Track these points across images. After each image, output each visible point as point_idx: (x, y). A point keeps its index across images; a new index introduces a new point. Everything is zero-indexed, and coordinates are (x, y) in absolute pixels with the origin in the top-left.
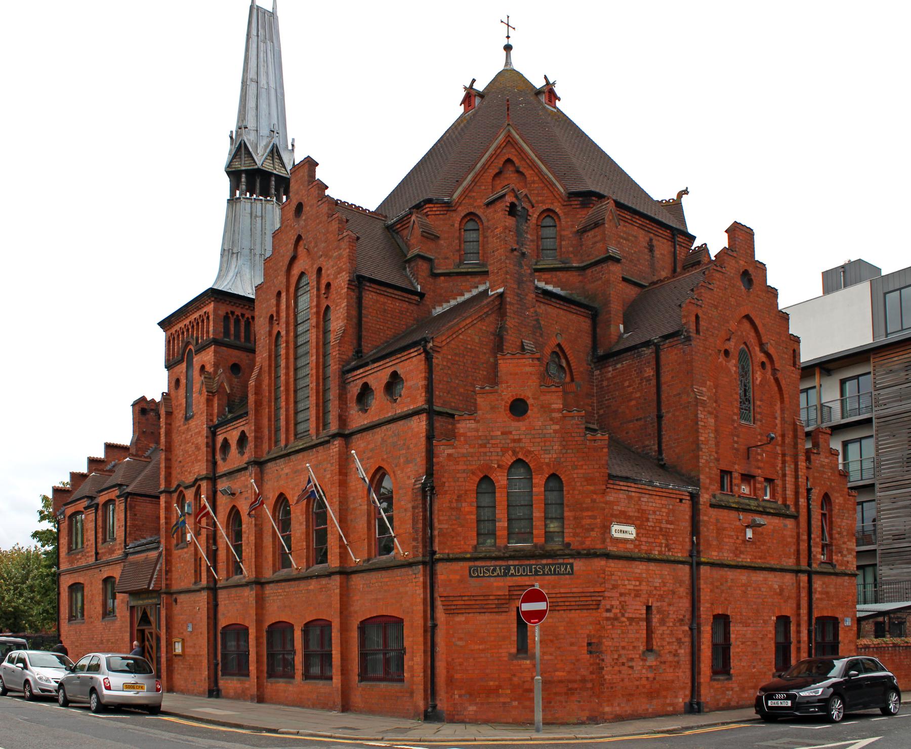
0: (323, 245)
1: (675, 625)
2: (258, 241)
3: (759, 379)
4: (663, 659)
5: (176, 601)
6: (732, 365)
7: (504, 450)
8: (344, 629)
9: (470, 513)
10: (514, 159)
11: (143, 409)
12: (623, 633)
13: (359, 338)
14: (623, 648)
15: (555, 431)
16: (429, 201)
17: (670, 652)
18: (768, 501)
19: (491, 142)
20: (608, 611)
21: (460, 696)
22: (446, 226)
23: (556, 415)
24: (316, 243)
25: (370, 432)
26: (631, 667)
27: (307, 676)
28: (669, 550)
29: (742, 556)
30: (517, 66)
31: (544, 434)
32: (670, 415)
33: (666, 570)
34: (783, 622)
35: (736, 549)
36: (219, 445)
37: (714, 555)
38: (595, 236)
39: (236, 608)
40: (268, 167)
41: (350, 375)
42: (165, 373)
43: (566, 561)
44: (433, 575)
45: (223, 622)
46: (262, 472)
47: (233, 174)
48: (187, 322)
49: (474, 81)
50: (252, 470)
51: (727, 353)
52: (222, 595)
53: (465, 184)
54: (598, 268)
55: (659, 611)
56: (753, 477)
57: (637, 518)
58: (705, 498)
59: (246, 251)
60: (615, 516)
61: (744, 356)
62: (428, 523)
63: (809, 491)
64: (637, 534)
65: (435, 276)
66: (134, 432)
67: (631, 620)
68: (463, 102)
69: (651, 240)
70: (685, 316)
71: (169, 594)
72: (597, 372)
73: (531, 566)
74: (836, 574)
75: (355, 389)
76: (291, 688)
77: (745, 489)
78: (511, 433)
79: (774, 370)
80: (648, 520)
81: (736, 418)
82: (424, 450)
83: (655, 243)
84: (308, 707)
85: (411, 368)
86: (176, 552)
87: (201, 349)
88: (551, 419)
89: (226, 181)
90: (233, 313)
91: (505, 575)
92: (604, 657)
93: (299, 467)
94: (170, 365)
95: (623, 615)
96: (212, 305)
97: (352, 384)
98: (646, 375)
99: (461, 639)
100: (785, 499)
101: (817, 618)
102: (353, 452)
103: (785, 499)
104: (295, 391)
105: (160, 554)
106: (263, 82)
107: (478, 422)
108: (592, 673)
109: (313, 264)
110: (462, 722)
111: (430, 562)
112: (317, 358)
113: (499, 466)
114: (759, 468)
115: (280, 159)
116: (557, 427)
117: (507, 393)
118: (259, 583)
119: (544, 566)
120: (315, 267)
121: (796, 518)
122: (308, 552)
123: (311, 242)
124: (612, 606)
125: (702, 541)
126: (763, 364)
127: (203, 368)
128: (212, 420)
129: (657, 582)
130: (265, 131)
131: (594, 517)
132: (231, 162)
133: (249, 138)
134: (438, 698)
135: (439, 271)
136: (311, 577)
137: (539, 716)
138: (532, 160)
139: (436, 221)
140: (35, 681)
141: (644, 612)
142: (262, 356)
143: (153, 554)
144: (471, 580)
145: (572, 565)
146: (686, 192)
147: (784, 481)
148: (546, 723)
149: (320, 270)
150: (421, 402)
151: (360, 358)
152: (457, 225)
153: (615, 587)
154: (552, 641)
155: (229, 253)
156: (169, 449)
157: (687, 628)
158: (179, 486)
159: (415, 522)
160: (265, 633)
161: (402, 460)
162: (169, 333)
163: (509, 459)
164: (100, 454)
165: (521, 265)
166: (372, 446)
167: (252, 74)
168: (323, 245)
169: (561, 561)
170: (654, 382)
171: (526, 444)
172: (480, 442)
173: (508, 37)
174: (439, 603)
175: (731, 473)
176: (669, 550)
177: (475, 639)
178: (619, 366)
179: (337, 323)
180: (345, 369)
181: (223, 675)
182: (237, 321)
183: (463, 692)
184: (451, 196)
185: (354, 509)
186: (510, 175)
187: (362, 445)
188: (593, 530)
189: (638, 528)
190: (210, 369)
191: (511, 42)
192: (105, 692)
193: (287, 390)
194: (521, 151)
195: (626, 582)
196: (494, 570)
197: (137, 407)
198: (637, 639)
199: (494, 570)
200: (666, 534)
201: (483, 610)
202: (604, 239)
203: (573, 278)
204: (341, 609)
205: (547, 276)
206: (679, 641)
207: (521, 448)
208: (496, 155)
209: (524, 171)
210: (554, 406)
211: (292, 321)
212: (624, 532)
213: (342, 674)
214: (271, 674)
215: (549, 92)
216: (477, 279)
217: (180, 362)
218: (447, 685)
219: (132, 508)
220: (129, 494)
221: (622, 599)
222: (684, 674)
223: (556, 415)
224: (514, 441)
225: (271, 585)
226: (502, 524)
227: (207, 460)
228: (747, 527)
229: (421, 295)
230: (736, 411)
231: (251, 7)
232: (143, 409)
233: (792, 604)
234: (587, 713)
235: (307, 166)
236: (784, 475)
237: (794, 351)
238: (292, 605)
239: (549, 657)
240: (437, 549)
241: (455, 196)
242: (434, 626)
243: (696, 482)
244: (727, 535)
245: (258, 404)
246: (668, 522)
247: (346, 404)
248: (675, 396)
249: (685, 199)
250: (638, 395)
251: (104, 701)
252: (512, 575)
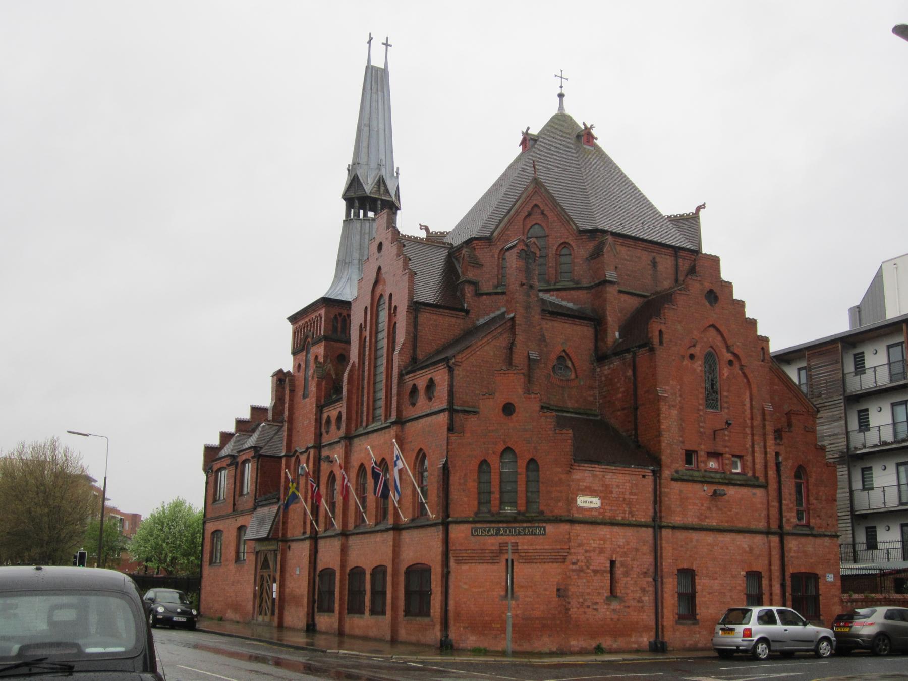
1: (638, 577)
3: (726, 375)
4: (627, 604)
5: (289, 548)
6: (698, 366)
8: (395, 574)
11: (281, 378)
12: (588, 582)
13: (415, 347)
14: (589, 594)
17: (634, 599)
18: (737, 474)
20: (574, 564)
26: (596, 610)
28: (632, 516)
29: (707, 520)
30: (568, 111)
33: (629, 532)
35: (701, 514)
36: (324, 421)
37: (677, 520)
39: (329, 554)
42: (291, 357)
45: (320, 567)
46: (350, 444)
48: (307, 320)
49: (528, 128)
51: (692, 357)
52: (321, 543)
55: (622, 565)
56: (721, 454)
57: (601, 492)
60: (582, 491)
61: (711, 358)
64: (602, 504)
67: (595, 572)
69: (654, 258)
72: (598, 370)
73: (515, 528)
74: (815, 536)
77: (713, 464)
79: (742, 367)
80: (612, 492)
81: (701, 407)
83: (658, 260)
85: (440, 376)
87: (315, 343)
89: (343, 203)
90: (340, 314)
91: (497, 534)
92: (570, 600)
94: (295, 353)
95: (588, 568)
99: (465, 583)
101: (793, 575)
106: (374, 123)
114: (726, 447)
118: (345, 534)
119: (524, 528)
121: (765, 486)
122: (377, 511)
124: (578, 561)
125: (663, 508)
126: (730, 363)
127: (316, 357)
128: (320, 401)
129: (621, 542)
130: (373, 165)
133: (361, 173)
136: (377, 531)
141: (608, 565)
144: (472, 538)
145: (544, 528)
146: (703, 206)
150: (445, 405)
151: (414, 364)
153: (580, 545)
155: (343, 263)
157: (651, 579)
162: (297, 325)
163: (501, 447)
165: (529, 296)
167: (366, 121)
169: (537, 525)
175: (696, 452)
176: (632, 516)
179: (401, 337)
188: (560, 501)
189: (602, 499)
190: (321, 360)
195: (592, 542)
198: (602, 587)
199: (489, 531)
200: (630, 504)
203: (582, 295)
205: (564, 293)
206: (643, 590)
212: (588, 502)
217: (302, 350)
221: (588, 555)
222: (648, 617)
226: (496, 495)
230: (701, 402)
231: (367, 68)
232: (281, 378)
236: (753, 452)
237: (763, 348)
239: (529, 599)
244: (687, 501)
246: (631, 494)
249: (702, 212)
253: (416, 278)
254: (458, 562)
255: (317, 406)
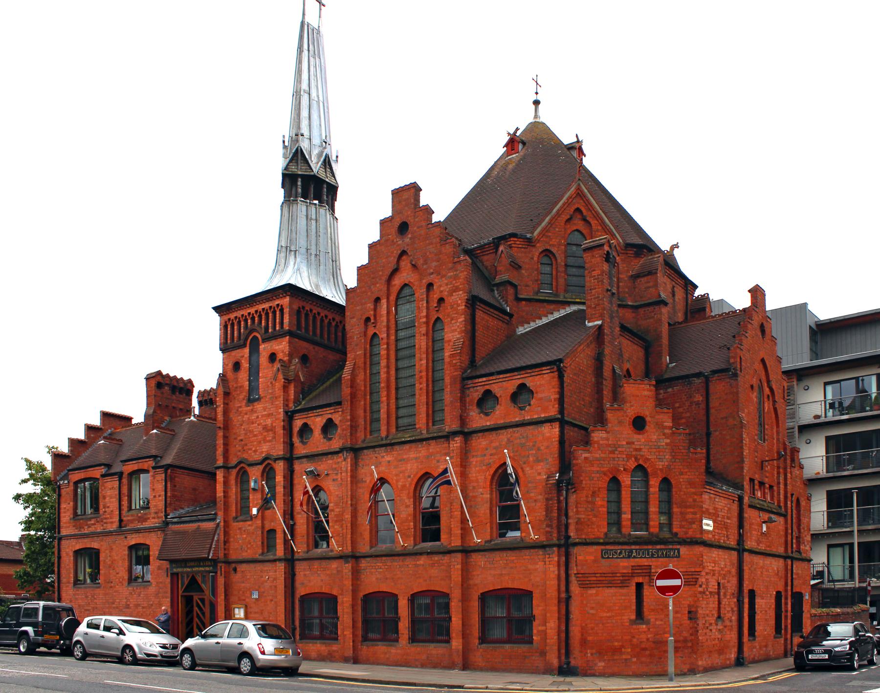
0: (434, 264)
2: (313, 242)
5: (235, 570)
7: (629, 457)
8: (465, 599)
9: (602, 506)
10: (583, 209)
15: (667, 444)
16: (513, 235)
19: (565, 193)
21: (592, 654)
22: (530, 258)
23: (667, 431)
24: (425, 261)
25: (494, 433)
27: (413, 639)
30: (542, 119)
31: (657, 445)
32: (717, 433)
34: (779, 594)
38: (648, 282)
40: (322, 175)
41: (470, 382)
42: (220, 355)
43: (674, 547)
44: (567, 555)
45: (301, 591)
47: (289, 179)
48: (252, 310)
50: (349, 456)
52: (300, 567)
53: (543, 224)
54: (651, 309)
57: (714, 514)
58: (746, 500)
59: (303, 250)
62: (563, 512)
63: (792, 495)
65: (518, 300)
66: (148, 404)
67: (711, 593)
68: (506, 145)
69: (674, 287)
70: (733, 357)
71: (228, 563)
73: (648, 550)
75: (476, 393)
76: (393, 650)
78: (633, 443)
82: (557, 452)
84: (417, 667)
86: (235, 525)
87: (275, 337)
88: (664, 434)
90: (304, 308)
91: (629, 557)
93: (405, 457)
96: (288, 299)
97: (472, 390)
98: (696, 400)
99: (592, 608)
100: (779, 502)
102: (506, 451)
103: (779, 502)
104: (397, 389)
105: (218, 525)
107: (608, 433)
108: (691, 635)
109: (421, 280)
110: (593, 675)
111: (566, 546)
112: (427, 363)
113: (625, 470)
115: (331, 168)
116: (668, 441)
117: (631, 411)
119: (658, 550)
120: (425, 282)
121: (785, 516)
123: (419, 259)
128: (287, 405)
130: (316, 141)
131: (695, 513)
132: (288, 165)
133: (304, 145)
134: (572, 656)
135: (522, 296)
137: (671, 669)
138: (596, 212)
139: (520, 255)
140: (139, 646)
142: (355, 353)
143: (210, 525)
145: (679, 550)
147: (779, 487)
148: (677, 675)
149: (430, 286)
152: (535, 259)
154: (662, 610)
156: (226, 427)
158: (240, 462)
159: (548, 510)
160: (360, 602)
161: (531, 459)
162: (226, 318)
163: (632, 464)
164: (96, 421)
166: (494, 445)
168: (434, 264)
169: (671, 547)
170: (703, 406)
171: (645, 452)
172: (610, 449)
173: (537, 93)
174: (573, 578)
177: (604, 608)
178: (670, 390)
180: (464, 375)
181: (301, 639)
182: (307, 315)
183: (594, 651)
184: (532, 233)
185: (474, 497)
186: (579, 224)
187: (484, 443)
188: (694, 523)
189: (714, 522)
191: (539, 98)
192: (261, 656)
193: (388, 387)
194: (588, 204)
196: (621, 553)
197: (153, 383)
199: (621, 553)
201: (610, 584)
202: (656, 285)
204: (462, 582)
206: (733, 611)
207: (642, 456)
208: (567, 204)
209: (590, 220)
210: (666, 424)
211: (393, 326)
213: (463, 638)
214: (365, 639)
215: (577, 148)
216: (552, 307)
218: (581, 645)
219: (172, 479)
220: (167, 467)
223: (667, 431)
224: (636, 450)
225: (368, 559)
227: (284, 442)
228: (764, 522)
229: (510, 315)
231: (303, 23)
233: (782, 583)
234: (687, 666)
235: (413, 190)
238: (402, 580)
240: (572, 534)
241: (536, 233)
242: (568, 599)
243: (741, 488)
245: (353, 396)
247: (465, 405)
248: (722, 418)
250: (688, 415)
251: (258, 664)
252: (634, 557)
253: (540, 106)
254: (585, 585)
255: (286, 413)
